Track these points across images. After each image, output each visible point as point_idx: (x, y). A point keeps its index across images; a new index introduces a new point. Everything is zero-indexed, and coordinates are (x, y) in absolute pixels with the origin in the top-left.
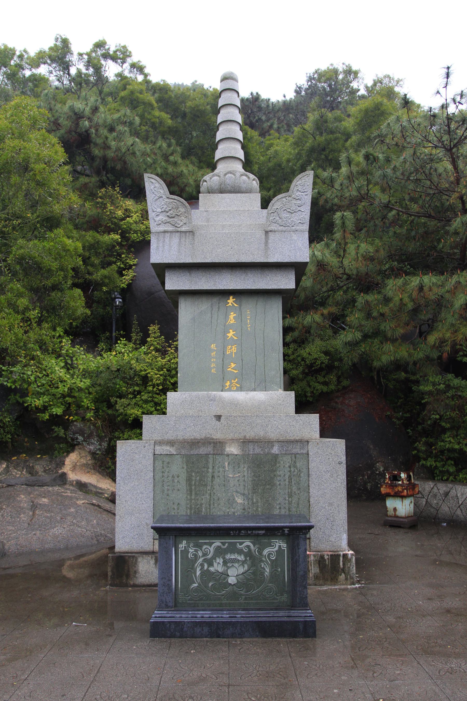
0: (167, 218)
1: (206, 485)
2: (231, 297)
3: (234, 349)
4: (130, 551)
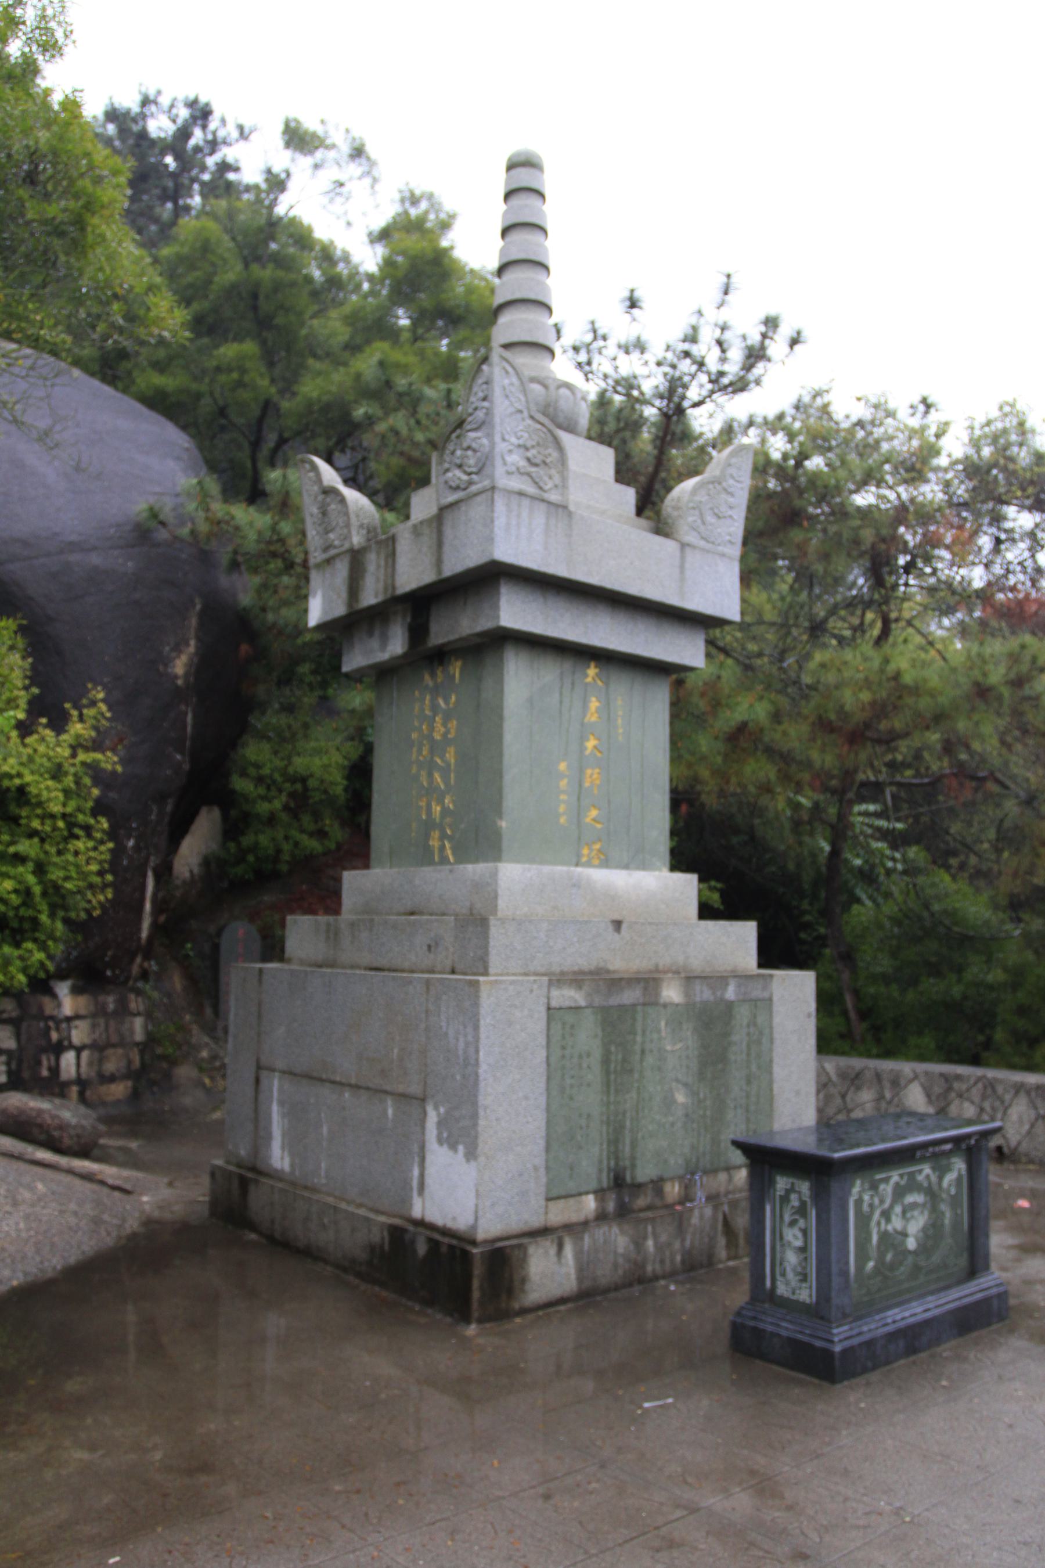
0: (523, 463)
1: (631, 1071)
4: (505, 1234)
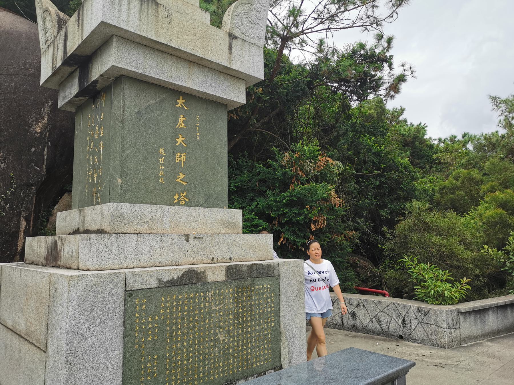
2: (181, 98)
3: (183, 158)
